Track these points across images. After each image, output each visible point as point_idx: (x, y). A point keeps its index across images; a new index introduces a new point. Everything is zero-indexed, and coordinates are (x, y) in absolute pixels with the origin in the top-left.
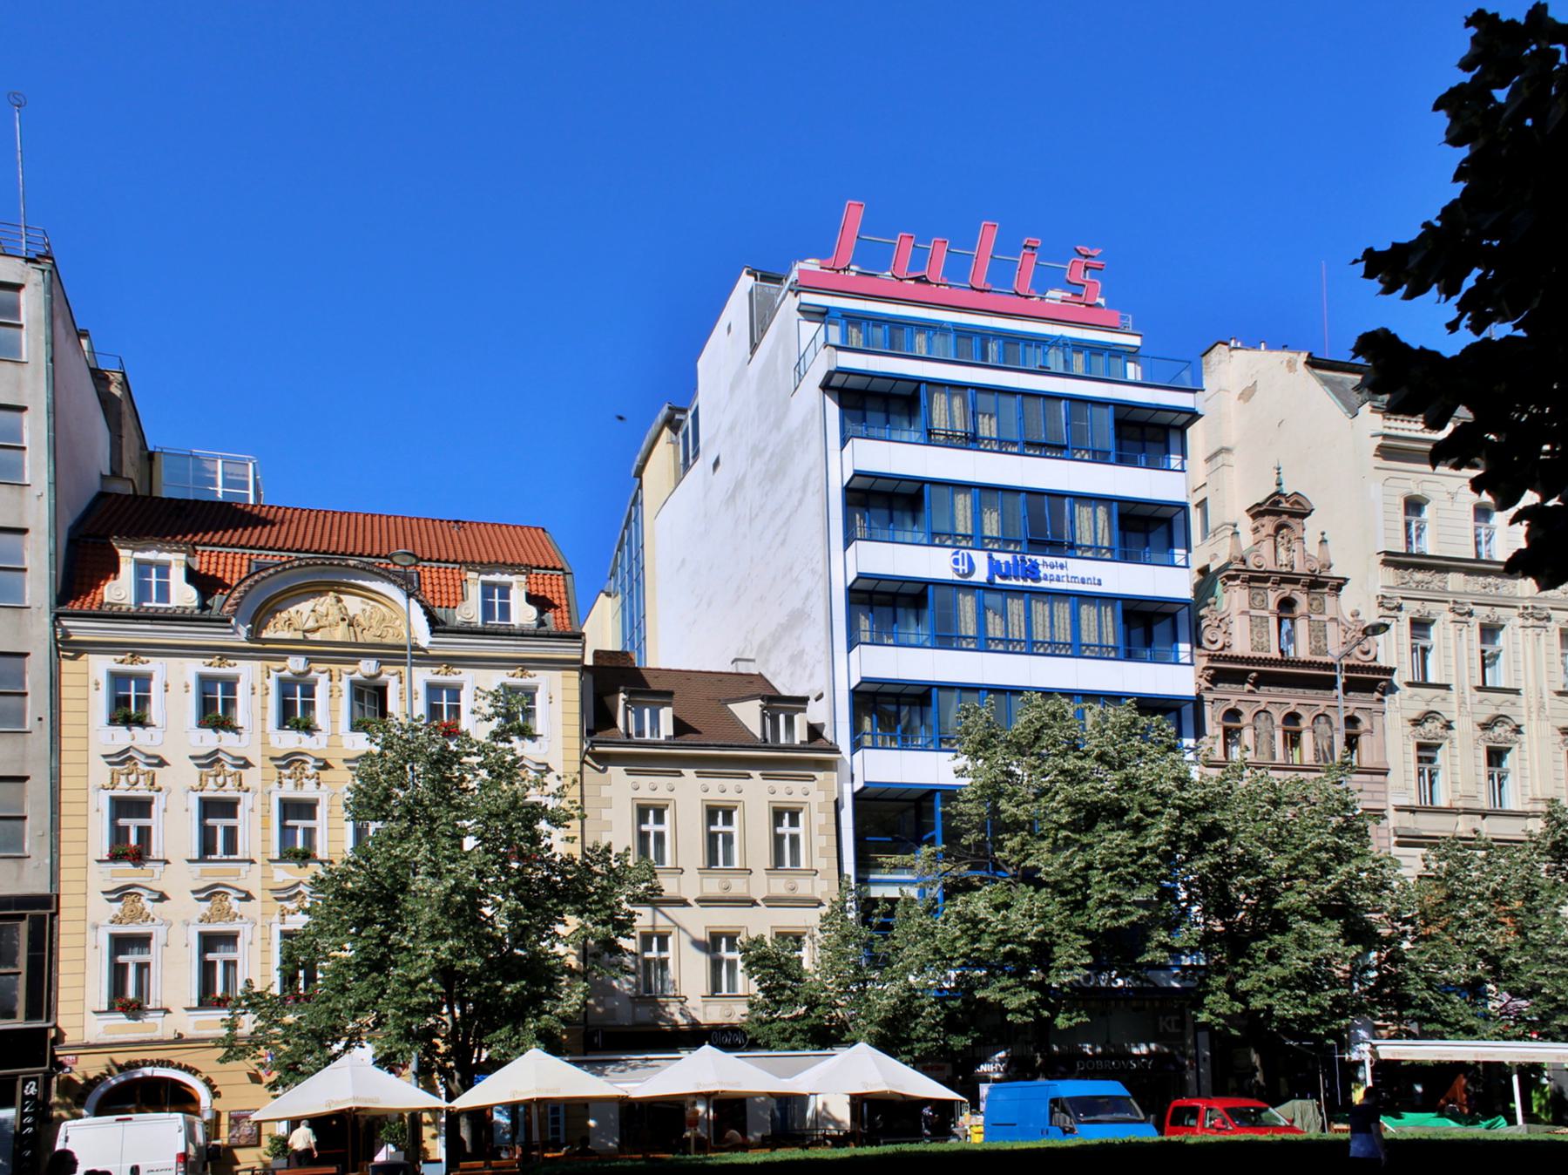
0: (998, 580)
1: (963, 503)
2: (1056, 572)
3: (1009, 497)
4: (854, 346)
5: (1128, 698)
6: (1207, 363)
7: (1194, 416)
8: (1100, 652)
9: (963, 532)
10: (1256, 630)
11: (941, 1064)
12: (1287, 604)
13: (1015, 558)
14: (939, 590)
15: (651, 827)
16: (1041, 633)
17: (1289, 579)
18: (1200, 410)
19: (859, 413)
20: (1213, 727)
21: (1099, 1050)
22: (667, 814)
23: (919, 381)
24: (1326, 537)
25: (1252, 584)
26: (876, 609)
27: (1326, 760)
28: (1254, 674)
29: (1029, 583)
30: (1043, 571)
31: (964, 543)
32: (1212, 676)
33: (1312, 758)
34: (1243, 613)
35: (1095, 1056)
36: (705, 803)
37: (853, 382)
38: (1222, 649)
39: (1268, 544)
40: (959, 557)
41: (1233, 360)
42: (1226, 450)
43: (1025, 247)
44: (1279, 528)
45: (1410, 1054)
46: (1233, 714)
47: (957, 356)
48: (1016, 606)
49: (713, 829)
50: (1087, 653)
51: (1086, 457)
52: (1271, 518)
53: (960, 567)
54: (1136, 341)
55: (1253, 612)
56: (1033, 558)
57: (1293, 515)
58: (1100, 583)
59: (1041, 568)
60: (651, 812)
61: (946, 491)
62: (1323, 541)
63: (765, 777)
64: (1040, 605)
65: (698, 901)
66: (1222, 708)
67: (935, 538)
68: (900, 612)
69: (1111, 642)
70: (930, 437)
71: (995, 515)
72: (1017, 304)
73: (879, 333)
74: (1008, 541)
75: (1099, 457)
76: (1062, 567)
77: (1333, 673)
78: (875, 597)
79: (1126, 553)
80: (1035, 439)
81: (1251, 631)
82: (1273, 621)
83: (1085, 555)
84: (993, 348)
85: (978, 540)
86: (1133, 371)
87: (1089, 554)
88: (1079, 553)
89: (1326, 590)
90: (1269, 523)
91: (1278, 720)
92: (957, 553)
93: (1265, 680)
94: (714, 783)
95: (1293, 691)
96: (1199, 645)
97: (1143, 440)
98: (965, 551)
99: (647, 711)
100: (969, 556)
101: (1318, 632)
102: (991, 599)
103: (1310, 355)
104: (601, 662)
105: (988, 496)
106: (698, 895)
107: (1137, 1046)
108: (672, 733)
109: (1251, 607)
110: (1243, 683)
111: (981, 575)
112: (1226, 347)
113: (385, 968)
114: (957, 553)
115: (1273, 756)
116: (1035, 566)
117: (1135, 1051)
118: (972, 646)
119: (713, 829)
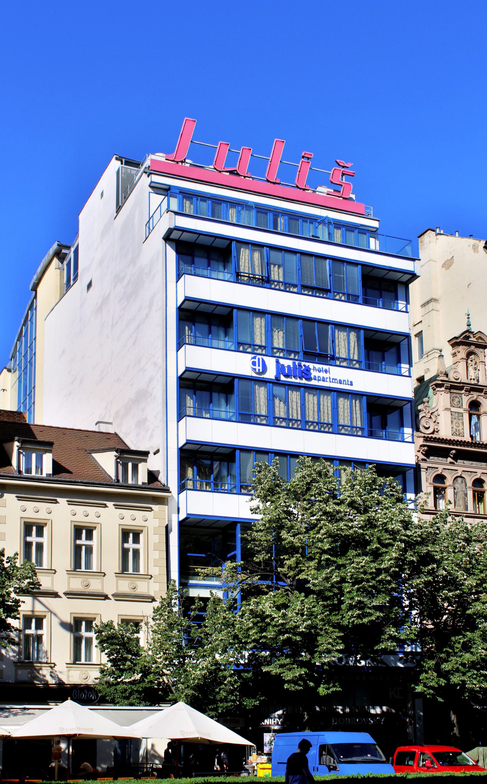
0: (283, 378)
2: (322, 375)
4: (187, 213)
7: (413, 276)
8: (352, 431)
10: (455, 421)
13: (294, 363)
15: (33, 539)
18: (417, 273)
22: (46, 530)
23: (231, 240)
25: (452, 391)
28: (454, 452)
29: (304, 381)
30: (314, 373)
34: (446, 409)
37: (186, 237)
38: (433, 433)
40: (257, 360)
43: (303, 157)
44: (469, 354)
48: (295, 396)
49: (78, 542)
50: (343, 431)
51: (343, 298)
52: (464, 347)
53: (257, 367)
54: (375, 224)
55: (453, 409)
56: (307, 364)
57: (478, 346)
58: (351, 384)
59: (312, 371)
60: (34, 528)
63: (117, 507)
64: (311, 397)
65: (66, 594)
66: (432, 474)
69: (359, 425)
70: (238, 278)
71: (281, 333)
72: (339, 203)
73: (205, 206)
74: (290, 352)
75: (352, 299)
76: (326, 371)
78: (197, 384)
80: (309, 284)
81: (452, 422)
82: (466, 416)
83: (342, 364)
84: (281, 221)
86: (373, 244)
87: (344, 364)
88: (338, 363)
90: (462, 351)
91: (469, 483)
92: (255, 358)
93: (461, 455)
95: (479, 464)
98: (260, 357)
99: (34, 455)
100: (263, 361)
102: (279, 391)
106: (66, 590)
107: (374, 708)
108: (51, 472)
109: (451, 406)
111: (271, 374)
114: (255, 358)
116: (308, 370)
117: (372, 711)
118: (264, 422)
119: (78, 542)
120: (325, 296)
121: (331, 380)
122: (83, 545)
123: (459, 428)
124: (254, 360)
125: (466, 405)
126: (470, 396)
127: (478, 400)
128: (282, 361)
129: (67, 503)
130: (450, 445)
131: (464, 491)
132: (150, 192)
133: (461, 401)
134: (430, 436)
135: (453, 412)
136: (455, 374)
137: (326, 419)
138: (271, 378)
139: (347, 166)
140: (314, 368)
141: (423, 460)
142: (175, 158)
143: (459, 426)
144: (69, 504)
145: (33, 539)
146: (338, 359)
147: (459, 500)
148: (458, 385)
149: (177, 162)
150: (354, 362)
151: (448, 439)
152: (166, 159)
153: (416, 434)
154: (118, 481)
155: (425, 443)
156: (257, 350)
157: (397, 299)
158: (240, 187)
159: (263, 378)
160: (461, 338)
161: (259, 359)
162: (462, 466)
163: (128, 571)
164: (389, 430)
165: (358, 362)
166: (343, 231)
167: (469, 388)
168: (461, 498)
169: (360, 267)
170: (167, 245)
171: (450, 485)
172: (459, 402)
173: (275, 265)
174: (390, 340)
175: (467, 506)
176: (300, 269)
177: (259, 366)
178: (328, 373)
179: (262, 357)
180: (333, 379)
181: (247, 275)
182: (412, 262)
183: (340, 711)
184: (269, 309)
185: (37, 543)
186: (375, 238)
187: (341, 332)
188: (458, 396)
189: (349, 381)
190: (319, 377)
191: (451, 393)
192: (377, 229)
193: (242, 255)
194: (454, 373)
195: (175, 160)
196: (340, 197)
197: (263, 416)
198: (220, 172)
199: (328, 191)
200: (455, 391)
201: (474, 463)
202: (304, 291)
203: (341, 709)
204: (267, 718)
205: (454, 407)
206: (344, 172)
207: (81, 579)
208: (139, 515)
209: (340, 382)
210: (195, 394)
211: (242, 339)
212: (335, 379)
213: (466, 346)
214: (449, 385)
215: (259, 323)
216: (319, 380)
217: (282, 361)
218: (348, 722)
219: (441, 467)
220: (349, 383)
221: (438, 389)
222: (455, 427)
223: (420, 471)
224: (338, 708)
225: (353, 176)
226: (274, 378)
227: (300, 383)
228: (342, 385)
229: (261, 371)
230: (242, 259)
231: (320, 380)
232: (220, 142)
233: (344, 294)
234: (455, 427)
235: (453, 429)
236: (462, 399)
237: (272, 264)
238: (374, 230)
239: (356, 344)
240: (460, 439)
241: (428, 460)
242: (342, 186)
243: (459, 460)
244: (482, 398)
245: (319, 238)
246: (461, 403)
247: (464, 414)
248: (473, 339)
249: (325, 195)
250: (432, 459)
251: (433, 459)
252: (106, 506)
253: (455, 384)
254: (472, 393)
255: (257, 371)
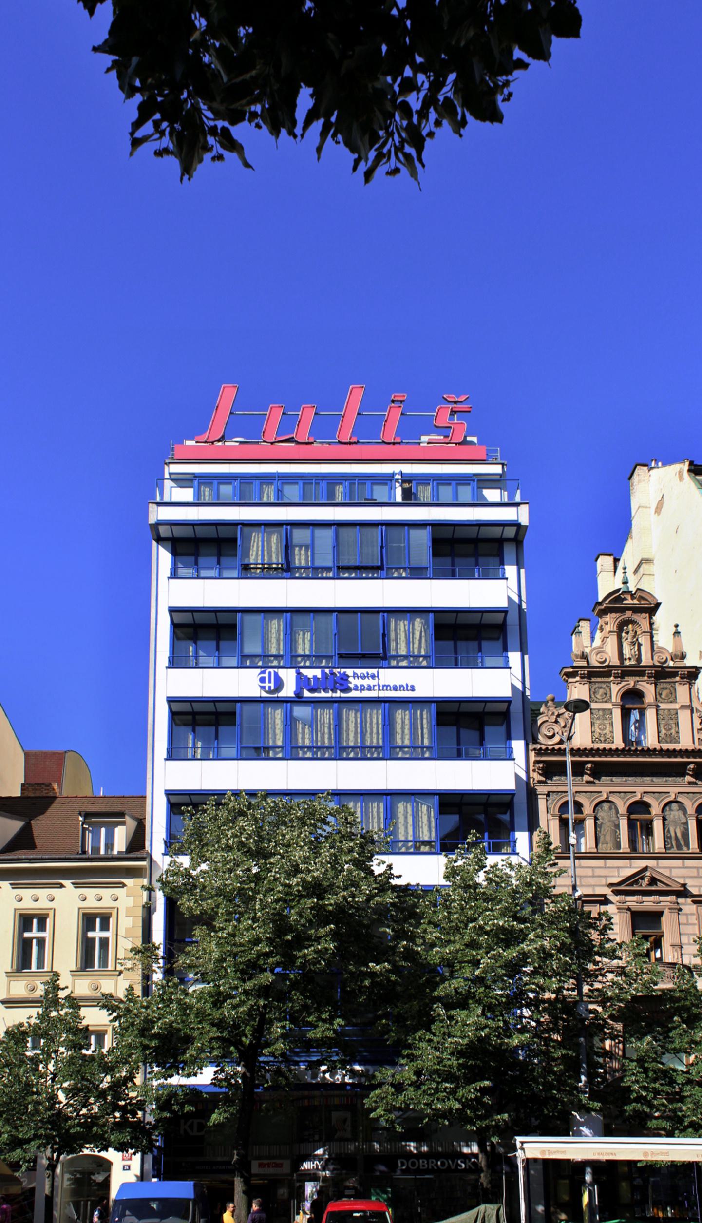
0: (307, 694)
1: (275, 626)
2: (366, 682)
3: (321, 618)
5: (214, 795)
6: (632, 484)
8: (415, 753)
9: (302, 653)
11: (278, 1161)
12: (633, 696)
13: (323, 673)
14: (247, 707)
15: (97, 934)
16: (351, 739)
17: (637, 672)
19: (192, 559)
20: (548, 822)
21: (425, 1149)
22: (49, 922)
24: (679, 629)
25: (593, 680)
26: (198, 729)
27: (679, 847)
28: (692, 766)
29: (338, 694)
30: (353, 682)
31: (275, 663)
32: (542, 769)
33: (662, 846)
35: (420, 1155)
36: (18, 912)
37: (178, 532)
39: (612, 641)
40: (266, 675)
41: (651, 478)
42: (648, 561)
43: (393, 401)
45: (564, 1152)
46: (640, 807)
47: (304, 500)
48: (326, 716)
49: (27, 935)
51: (404, 575)
52: (614, 615)
53: (267, 685)
54: (497, 469)
56: (343, 671)
57: (636, 610)
58: (413, 689)
59: (351, 679)
60: (98, 920)
61: (259, 617)
62: (677, 633)
63: (77, 885)
64: (352, 715)
66: (556, 803)
67: (244, 661)
68: (488, 729)
69: (426, 743)
70: (246, 571)
71: (308, 636)
72: (452, 450)
73: (226, 490)
74: (319, 657)
75: (417, 573)
76: (373, 677)
77: (574, 759)
78: (197, 717)
79: (438, 661)
81: (592, 724)
82: (617, 714)
83: (401, 664)
84: (340, 490)
85: (291, 660)
86: (492, 495)
87: (404, 663)
88: (394, 663)
89: (678, 679)
91: (623, 809)
93: (600, 771)
94: (26, 893)
95: (639, 780)
96: (535, 741)
97: (476, 555)
98: (272, 670)
99: (103, 830)
100: (276, 674)
101: (666, 722)
102: (300, 711)
103: (691, 463)
104: (26, 794)
105: (299, 618)
107: (468, 1146)
108: (124, 850)
110: (683, 775)
112: (646, 468)
113: (310, 1069)
114: (264, 672)
115: (618, 845)
116: (345, 678)
117: (466, 1150)
118: (280, 755)
119: (27, 935)
120: (375, 575)
121: (381, 688)
122: (34, 938)
123: (604, 732)
124: (262, 675)
125: (615, 697)
126: (623, 683)
127: (638, 687)
128: (304, 672)
129: (10, 887)
130: (580, 756)
131: (613, 822)
132: (171, 487)
133: (609, 693)
134: (557, 747)
135: (595, 709)
136: (599, 656)
137: (326, 741)
138: (289, 695)
139: (460, 400)
140: (355, 676)
141: (540, 782)
142: (350, 439)
143: (605, 729)
144: (13, 888)
145: (97, 934)
146: (395, 657)
147: (605, 835)
148: (601, 670)
149: (213, 443)
150: (421, 659)
151: (588, 748)
152: (197, 442)
153: (531, 747)
154: (84, 852)
155: (538, 759)
156: (272, 662)
157: (502, 563)
158: (298, 458)
159: (278, 697)
160: (607, 602)
161: (270, 673)
162: (606, 787)
163: (30, 969)
164: (489, 746)
165: (425, 657)
166: (473, 488)
167: (619, 672)
168: (609, 832)
169: (429, 528)
170: (160, 547)
171: (656, 815)
172: (606, 694)
173: (300, 547)
174: (460, 621)
175: (619, 842)
176: (336, 546)
177: (270, 682)
178: (376, 678)
179: (276, 670)
180: (383, 686)
181: (260, 566)
182: (514, 509)
183: (412, 1149)
184: (433, 605)
185: (101, 939)
186: (501, 488)
187: (400, 621)
188: (604, 686)
189: (409, 685)
190: (361, 686)
191: (590, 682)
192: (501, 475)
193: (254, 542)
194: (597, 654)
195: (208, 441)
196: (447, 443)
197: (279, 747)
198: (272, 443)
199: (429, 439)
200: (599, 679)
201: (630, 778)
202: (344, 574)
203: (414, 1147)
204: (305, 1161)
205: (596, 702)
206: (454, 410)
207: (89, 981)
208: (106, 893)
209: (395, 688)
210: (194, 731)
211: (247, 650)
212: (387, 686)
213: (616, 613)
214: (619, 672)
215: (275, 626)
216: (361, 690)
217: (304, 672)
218: (424, 1166)
219: (673, 791)
220: (409, 688)
221: (570, 680)
222: (598, 731)
223: (537, 799)
224: (409, 1146)
225: (469, 412)
226: (294, 696)
227: (332, 697)
228: (399, 692)
229: (272, 688)
230: (253, 546)
231: (364, 690)
232: (271, 406)
233: (405, 569)
234: (598, 731)
235: (595, 734)
236: (675, 690)
237: (297, 546)
238: (498, 477)
239: (423, 634)
240: (607, 746)
241: (597, 782)
242: (451, 427)
243: (603, 778)
244: (644, 684)
245: (376, 500)
246: (608, 695)
247: (613, 710)
248: (629, 601)
249: (426, 445)
250: (557, 780)
251: (559, 780)
252: (62, 886)
253: (595, 670)
254: (626, 678)
255: (267, 689)
